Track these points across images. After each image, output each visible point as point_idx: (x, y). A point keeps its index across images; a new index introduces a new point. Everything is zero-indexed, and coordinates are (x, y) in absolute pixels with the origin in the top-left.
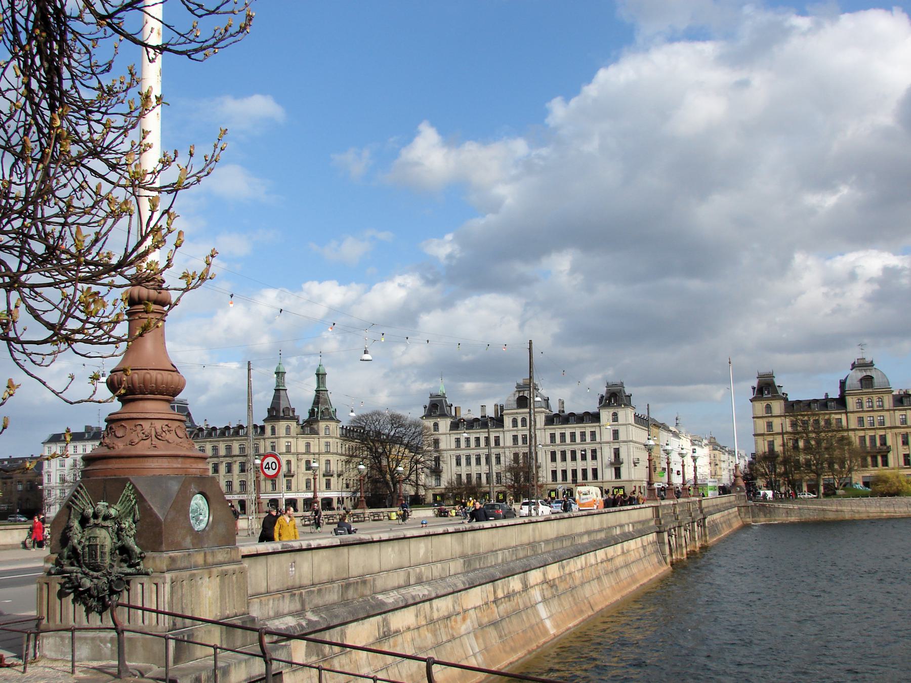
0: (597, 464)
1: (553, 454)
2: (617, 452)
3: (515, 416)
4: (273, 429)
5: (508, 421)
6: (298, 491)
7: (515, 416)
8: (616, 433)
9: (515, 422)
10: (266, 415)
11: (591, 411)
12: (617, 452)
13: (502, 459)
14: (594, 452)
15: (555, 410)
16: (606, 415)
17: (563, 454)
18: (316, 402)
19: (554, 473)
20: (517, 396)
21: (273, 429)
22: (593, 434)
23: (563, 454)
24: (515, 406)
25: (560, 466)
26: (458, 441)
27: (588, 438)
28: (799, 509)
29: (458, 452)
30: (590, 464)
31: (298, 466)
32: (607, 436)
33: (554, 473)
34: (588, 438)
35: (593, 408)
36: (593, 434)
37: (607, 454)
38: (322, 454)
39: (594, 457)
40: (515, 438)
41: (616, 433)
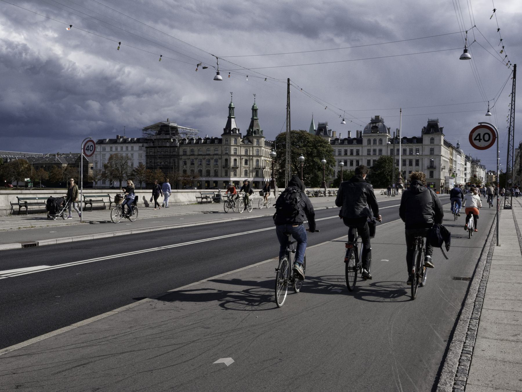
4: (432, 140)
5: (365, 141)
8: (432, 150)
9: (369, 141)
12: (432, 162)
13: (420, 163)
16: (427, 139)
18: (252, 126)
21: (432, 140)
32: (427, 151)
35: (419, 134)
37: (426, 163)
38: (224, 155)
39: (417, 164)
40: (369, 151)
41: (432, 150)
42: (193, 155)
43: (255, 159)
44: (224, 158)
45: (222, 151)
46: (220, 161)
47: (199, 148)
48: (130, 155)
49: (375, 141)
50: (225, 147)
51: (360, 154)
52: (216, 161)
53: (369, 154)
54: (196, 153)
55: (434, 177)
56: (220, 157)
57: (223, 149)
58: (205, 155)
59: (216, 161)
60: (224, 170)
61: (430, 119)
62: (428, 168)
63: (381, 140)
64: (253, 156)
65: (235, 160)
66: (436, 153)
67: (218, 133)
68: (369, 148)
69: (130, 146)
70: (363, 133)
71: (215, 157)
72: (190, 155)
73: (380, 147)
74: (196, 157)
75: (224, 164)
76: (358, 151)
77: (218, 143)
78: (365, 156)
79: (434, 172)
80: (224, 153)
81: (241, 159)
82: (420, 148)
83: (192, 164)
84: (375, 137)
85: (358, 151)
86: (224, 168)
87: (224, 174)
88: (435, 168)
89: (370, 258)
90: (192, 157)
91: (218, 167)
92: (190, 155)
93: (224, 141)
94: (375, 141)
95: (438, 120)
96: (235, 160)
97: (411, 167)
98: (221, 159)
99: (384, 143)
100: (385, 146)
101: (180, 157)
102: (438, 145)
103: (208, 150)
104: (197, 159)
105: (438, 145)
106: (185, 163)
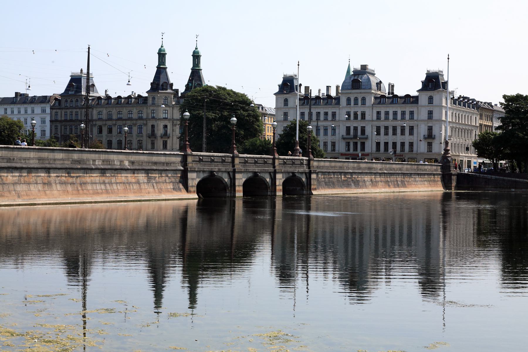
0: (414, 139)
1: (378, 129)
2: (430, 129)
3: (349, 96)
4: (431, 99)
6: (172, 150)
7: (349, 96)
8: (430, 113)
9: (349, 100)
10: (420, 86)
11: (412, 95)
12: (430, 129)
13: (337, 131)
14: (411, 128)
15: (386, 90)
17: (395, 129)
19: (378, 144)
20: (352, 79)
21: (431, 99)
22: (412, 113)
23: (395, 129)
24: (350, 87)
25: (382, 139)
26: (378, 113)
27: (407, 116)
28: (496, 179)
29: (378, 124)
30: (407, 138)
31: (173, 130)
32: (424, 115)
33: (378, 144)
34: (407, 116)
36: (412, 113)
37: (423, 130)
38: (150, 120)
39: (411, 133)
41: (430, 113)
42: (110, 119)
43: (150, 123)
44: (150, 123)
45: (147, 114)
46: (144, 128)
47: (129, 109)
48: (22, 120)
49: (356, 99)
50: (152, 108)
51: (337, 118)
52: (140, 128)
53: (378, 118)
54: (114, 117)
55: (433, 151)
56: (145, 122)
57: (149, 111)
58: (126, 120)
59: (140, 128)
60: (149, 141)
61: (285, 74)
62: (425, 138)
63: (364, 99)
64: (146, 119)
65: (165, 127)
66: (435, 116)
67: (143, 88)
68: (349, 110)
69: (29, 108)
70: (340, 88)
71: (139, 122)
72: (106, 120)
73: (363, 109)
74: (114, 122)
75: (150, 132)
76: (334, 114)
77: (143, 103)
78: (343, 121)
79: (168, 142)
80: (150, 117)
81: (174, 125)
82: (415, 110)
83: (110, 131)
84: (356, 95)
85: (334, 114)
86: (149, 137)
87: (149, 146)
88: (434, 138)
89: (123, 262)
90: (109, 123)
91: (142, 136)
92: (106, 120)
93: (150, 101)
94: (356, 99)
95: (428, 71)
96: (165, 127)
97: (403, 137)
98: (146, 125)
99: (368, 104)
100: (369, 107)
101: (94, 123)
102: (438, 106)
103: (130, 112)
104: (116, 124)
105: (438, 106)
106: (100, 131)
